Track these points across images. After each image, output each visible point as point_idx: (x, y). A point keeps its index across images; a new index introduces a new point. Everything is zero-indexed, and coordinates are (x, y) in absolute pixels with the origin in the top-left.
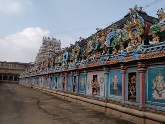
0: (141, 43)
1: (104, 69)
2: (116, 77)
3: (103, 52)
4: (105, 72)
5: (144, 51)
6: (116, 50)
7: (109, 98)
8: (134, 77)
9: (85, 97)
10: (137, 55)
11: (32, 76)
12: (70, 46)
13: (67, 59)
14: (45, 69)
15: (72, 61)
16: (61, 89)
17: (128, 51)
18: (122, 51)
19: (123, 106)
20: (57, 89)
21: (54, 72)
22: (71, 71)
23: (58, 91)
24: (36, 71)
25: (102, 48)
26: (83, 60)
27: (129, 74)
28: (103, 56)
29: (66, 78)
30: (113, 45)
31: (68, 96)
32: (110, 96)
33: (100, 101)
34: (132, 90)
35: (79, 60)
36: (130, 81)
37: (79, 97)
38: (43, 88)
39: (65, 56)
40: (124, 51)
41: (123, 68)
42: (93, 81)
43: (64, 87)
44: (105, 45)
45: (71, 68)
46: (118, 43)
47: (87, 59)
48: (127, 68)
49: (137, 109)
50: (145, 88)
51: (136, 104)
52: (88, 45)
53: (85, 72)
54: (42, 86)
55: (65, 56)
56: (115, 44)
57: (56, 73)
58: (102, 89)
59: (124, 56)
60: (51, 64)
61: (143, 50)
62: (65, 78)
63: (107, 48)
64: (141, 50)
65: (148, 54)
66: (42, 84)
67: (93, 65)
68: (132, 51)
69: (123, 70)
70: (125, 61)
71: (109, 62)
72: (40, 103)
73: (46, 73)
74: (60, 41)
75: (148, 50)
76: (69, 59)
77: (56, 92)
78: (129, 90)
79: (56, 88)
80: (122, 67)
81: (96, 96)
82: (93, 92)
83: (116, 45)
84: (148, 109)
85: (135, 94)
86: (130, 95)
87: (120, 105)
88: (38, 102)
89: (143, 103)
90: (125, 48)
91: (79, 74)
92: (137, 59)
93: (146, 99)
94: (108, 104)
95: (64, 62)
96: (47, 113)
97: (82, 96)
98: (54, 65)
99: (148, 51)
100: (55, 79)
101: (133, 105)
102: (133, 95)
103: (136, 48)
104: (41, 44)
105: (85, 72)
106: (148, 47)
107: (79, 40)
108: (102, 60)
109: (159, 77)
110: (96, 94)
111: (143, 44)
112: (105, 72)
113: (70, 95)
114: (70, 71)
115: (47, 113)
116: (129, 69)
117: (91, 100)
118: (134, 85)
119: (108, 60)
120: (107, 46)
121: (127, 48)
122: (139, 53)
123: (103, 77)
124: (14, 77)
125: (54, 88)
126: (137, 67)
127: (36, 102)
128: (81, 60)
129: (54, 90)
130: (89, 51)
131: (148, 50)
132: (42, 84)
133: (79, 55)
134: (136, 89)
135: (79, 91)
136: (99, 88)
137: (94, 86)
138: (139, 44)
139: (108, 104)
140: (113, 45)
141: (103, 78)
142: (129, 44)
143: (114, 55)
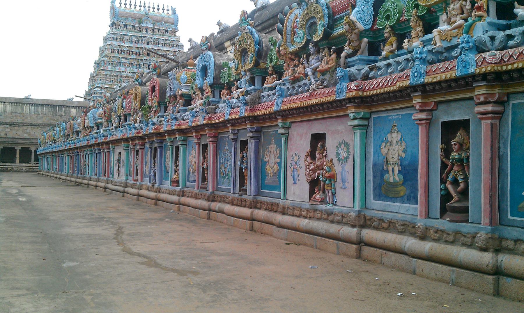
0: (487, 11)
1: (351, 112)
2: (395, 137)
3: (347, 50)
4: (356, 122)
5: (497, 42)
6: (393, 39)
7: (369, 213)
8: (460, 135)
9: (284, 213)
10: (472, 57)
11: (85, 143)
12: (216, 30)
13: (210, 79)
14: (130, 121)
15: (230, 86)
16: (193, 187)
17: (439, 44)
18: (416, 43)
19: (423, 238)
20: (178, 189)
21: (164, 128)
22: (229, 121)
23: (182, 194)
24: (98, 125)
25: (342, 35)
26: (270, 82)
27: (443, 124)
28: (347, 65)
29: (211, 148)
30: (381, 22)
31: (222, 212)
32: (376, 204)
33: (339, 222)
34: (455, 182)
35: (257, 81)
36: (447, 151)
37: (261, 213)
38: (126, 185)
39: (204, 69)
40: (425, 43)
41: (424, 104)
42: (312, 155)
43: (204, 180)
44: (352, 25)
45: (227, 110)
46: (400, 13)
47: (285, 77)
48: (438, 103)
49: (470, 246)
50: (501, 170)
51: (465, 228)
52: (289, 24)
53: (280, 122)
54: (123, 179)
55: (204, 69)
56: (388, 18)
57: (171, 133)
58: (343, 181)
59: (424, 61)
60: (153, 101)
61: (492, 38)
62: (205, 146)
63: (361, 34)
64: (486, 38)
65: (511, 51)
66: (123, 170)
67: (311, 96)
68: (455, 42)
69: (422, 111)
70: (428, 79)
71: (369, 84)
72: (124, 237)
73: (133, 133)
74: (174, 12)
75: (510, 37)
76: (217, 78)
77: (175, 198)
78: (443, 181)
79: (176, 183)
80: (417, 101)
81: (324, 207)
82: (312, 192)
83: (392, 22)
84: (511, 244)
85: (464, 194)
86: (446, 197)
87: (413, 235)
88: (119, 231)
89: (491, 224)
90: (428, 30)
91: (258, 131)
92: (472, 70)
93: (501, 211)
94: (369, 234)
95: (202, 90)
96: (157, 265)
97: (272, 208)
98: (163, 104)
99: (511, 43)
100: (169, 154)
101: (457, 233)
102: (456, 198)
103: (469, 30)
104: (105, 29)
105: (280, 122)
106: (509, 27)
107: (250, 8)
108: (342, 78)
109: (394, 135)
110: (323, 201)
111: (492, 18)
112: (356, 122)
113: (228, 208)
114: (224, 124)
115: (157, 265)
116: (441, 107)
117: (304, 223)
118: (463, 164)
119: (366, 77)
120: (361, 26)
121: (435, 32)
122: (480, 48)
123: (348, 139)
124: (18, 149)
125: (167, 185)
126: (471, 99)
127: (113, 231)
128: (263, 81)
129: (171, 193)
130: (292, 49)
131: (510, 37)
132: (123, 170)
133: (257, 64)
134: (466, 179)
135: (258, 193)
136: (332, 178)
137: (314, 171)
138: (481, 17)
139: (369, 234)
140: (381, 22)
141: (347, 145)
142: (443, 17)
143: (386, 58)
